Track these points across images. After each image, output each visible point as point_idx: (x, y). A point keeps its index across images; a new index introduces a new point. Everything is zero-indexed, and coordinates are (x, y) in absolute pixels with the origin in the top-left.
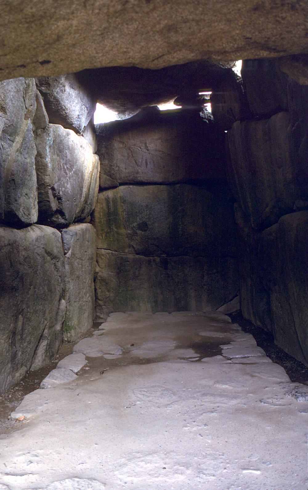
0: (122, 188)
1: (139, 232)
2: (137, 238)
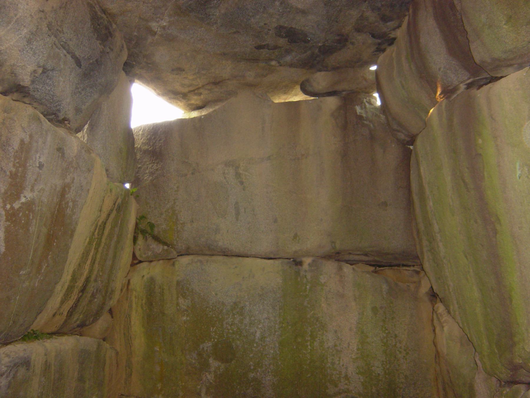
0: (185, 260)
1: (214, 363)
2: (209, 377)
